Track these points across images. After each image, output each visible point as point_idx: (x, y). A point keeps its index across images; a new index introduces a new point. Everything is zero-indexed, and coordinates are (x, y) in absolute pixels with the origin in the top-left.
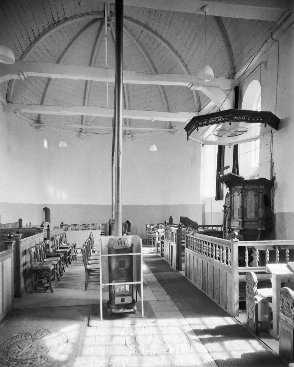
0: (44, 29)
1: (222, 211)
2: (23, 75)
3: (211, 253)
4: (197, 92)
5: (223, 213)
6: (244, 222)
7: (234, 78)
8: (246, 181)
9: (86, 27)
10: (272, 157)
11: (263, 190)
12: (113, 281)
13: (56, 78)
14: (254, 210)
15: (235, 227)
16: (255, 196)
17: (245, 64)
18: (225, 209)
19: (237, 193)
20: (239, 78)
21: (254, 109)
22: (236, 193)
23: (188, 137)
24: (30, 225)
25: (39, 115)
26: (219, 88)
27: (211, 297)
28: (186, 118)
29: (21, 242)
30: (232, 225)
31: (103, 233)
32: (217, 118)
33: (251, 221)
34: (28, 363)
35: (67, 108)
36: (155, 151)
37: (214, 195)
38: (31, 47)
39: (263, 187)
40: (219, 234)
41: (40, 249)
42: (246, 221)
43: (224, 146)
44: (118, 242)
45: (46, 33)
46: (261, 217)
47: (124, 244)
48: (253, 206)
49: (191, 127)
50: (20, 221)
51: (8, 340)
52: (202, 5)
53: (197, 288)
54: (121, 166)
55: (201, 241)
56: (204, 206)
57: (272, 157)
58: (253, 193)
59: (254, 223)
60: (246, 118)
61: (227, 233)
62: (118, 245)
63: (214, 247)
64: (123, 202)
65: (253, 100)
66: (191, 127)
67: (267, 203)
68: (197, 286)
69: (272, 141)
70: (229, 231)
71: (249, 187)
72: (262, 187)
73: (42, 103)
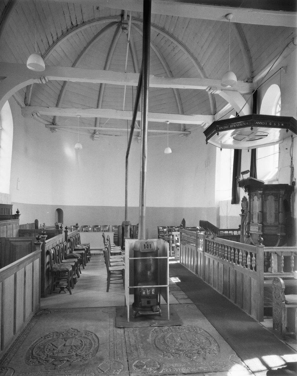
0: (62, 33)
1: (240, 215)
2: (45, 79)
3: (233, 257)
4: (213, 95)
5: (240, 218)
6: (263, 226)
7: (252, 82)
8: (267, 185)
9: (103, 30)
10: (292, 162)
11: (283, 195)
12: (139, 284)
13: (76, 82)
14: (273, 215)
15: (254, 232)
16: (275, 200)
17: (264, 68)
18: (242, 214)
19: (257, 198)
20: (257, 82)
21: (273, 114)
22: (256, 198)
23: (207, 141)
24: (44, 226)
25: (55, 117)
26: (237, 91)
27: (233, 302)
28: (205, 121)
29: (46, 243)
30: (251, 230)
31: (116, 235)
32: (238, 123)
33: (271, 226)
34: (65, 360)
35: (83, 110)
36: (171, 154)
37: (230, 198)
38: (50, 51)
39: (284, 192)
40: (237, 238)
41: (58, 251)
42: (266, 226)
43: (241, 150)
44: (144, 245)
45: (64, 37)
46: (281, 221)
47: (151, 248)
48: (273, 211)
49: (210, 131)
50: (36, 221)
51: (41, 337)
52: (226, 13)
53: (218, 292)
54: (145, 170)
55: (222, 245)
56: (218, 209)
57: (292, 162)
58: (273, 198)
59: (274, 228)
60: (268, 123)
61: (245, 238)
62: (145, 248)
63: (237, 252)
64: (147, 204)
65: (271, 104)
66: (210, 131)
67: (287, 207)
68: (217, 291)
69: (292, 146)
70: (248, 235)
71: (269, 192)
72: (282, 192)
73: (57, 105)
